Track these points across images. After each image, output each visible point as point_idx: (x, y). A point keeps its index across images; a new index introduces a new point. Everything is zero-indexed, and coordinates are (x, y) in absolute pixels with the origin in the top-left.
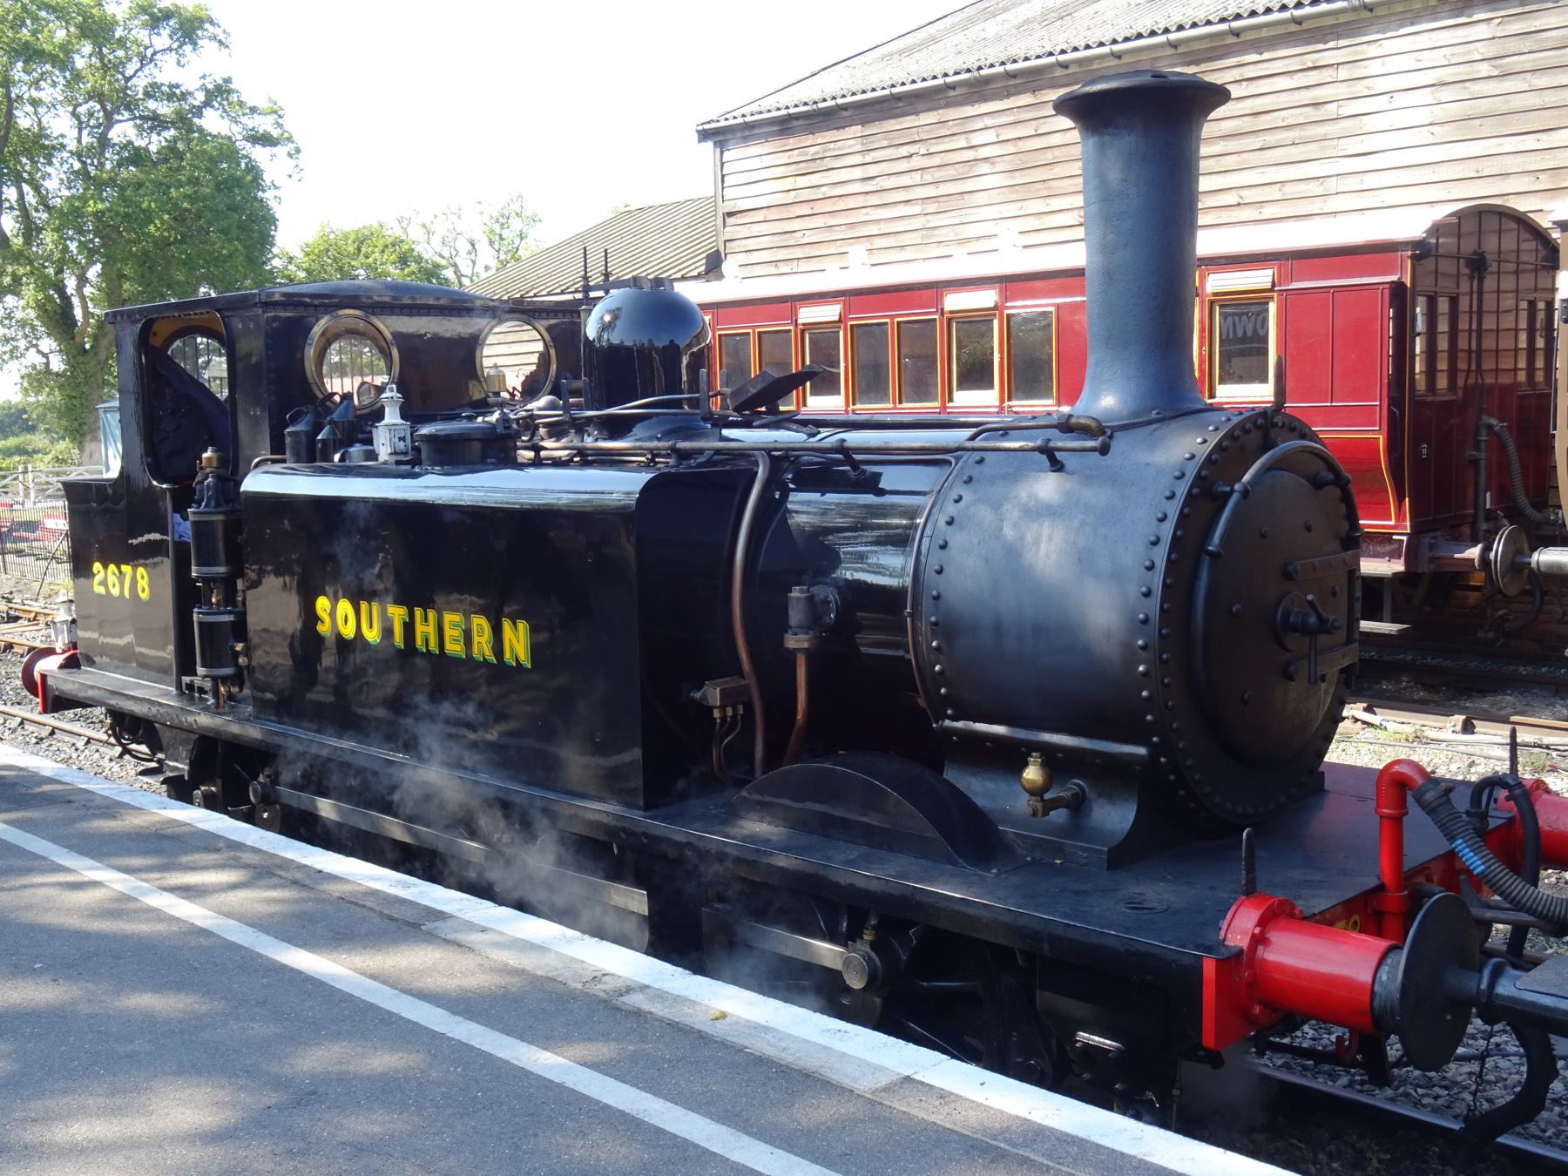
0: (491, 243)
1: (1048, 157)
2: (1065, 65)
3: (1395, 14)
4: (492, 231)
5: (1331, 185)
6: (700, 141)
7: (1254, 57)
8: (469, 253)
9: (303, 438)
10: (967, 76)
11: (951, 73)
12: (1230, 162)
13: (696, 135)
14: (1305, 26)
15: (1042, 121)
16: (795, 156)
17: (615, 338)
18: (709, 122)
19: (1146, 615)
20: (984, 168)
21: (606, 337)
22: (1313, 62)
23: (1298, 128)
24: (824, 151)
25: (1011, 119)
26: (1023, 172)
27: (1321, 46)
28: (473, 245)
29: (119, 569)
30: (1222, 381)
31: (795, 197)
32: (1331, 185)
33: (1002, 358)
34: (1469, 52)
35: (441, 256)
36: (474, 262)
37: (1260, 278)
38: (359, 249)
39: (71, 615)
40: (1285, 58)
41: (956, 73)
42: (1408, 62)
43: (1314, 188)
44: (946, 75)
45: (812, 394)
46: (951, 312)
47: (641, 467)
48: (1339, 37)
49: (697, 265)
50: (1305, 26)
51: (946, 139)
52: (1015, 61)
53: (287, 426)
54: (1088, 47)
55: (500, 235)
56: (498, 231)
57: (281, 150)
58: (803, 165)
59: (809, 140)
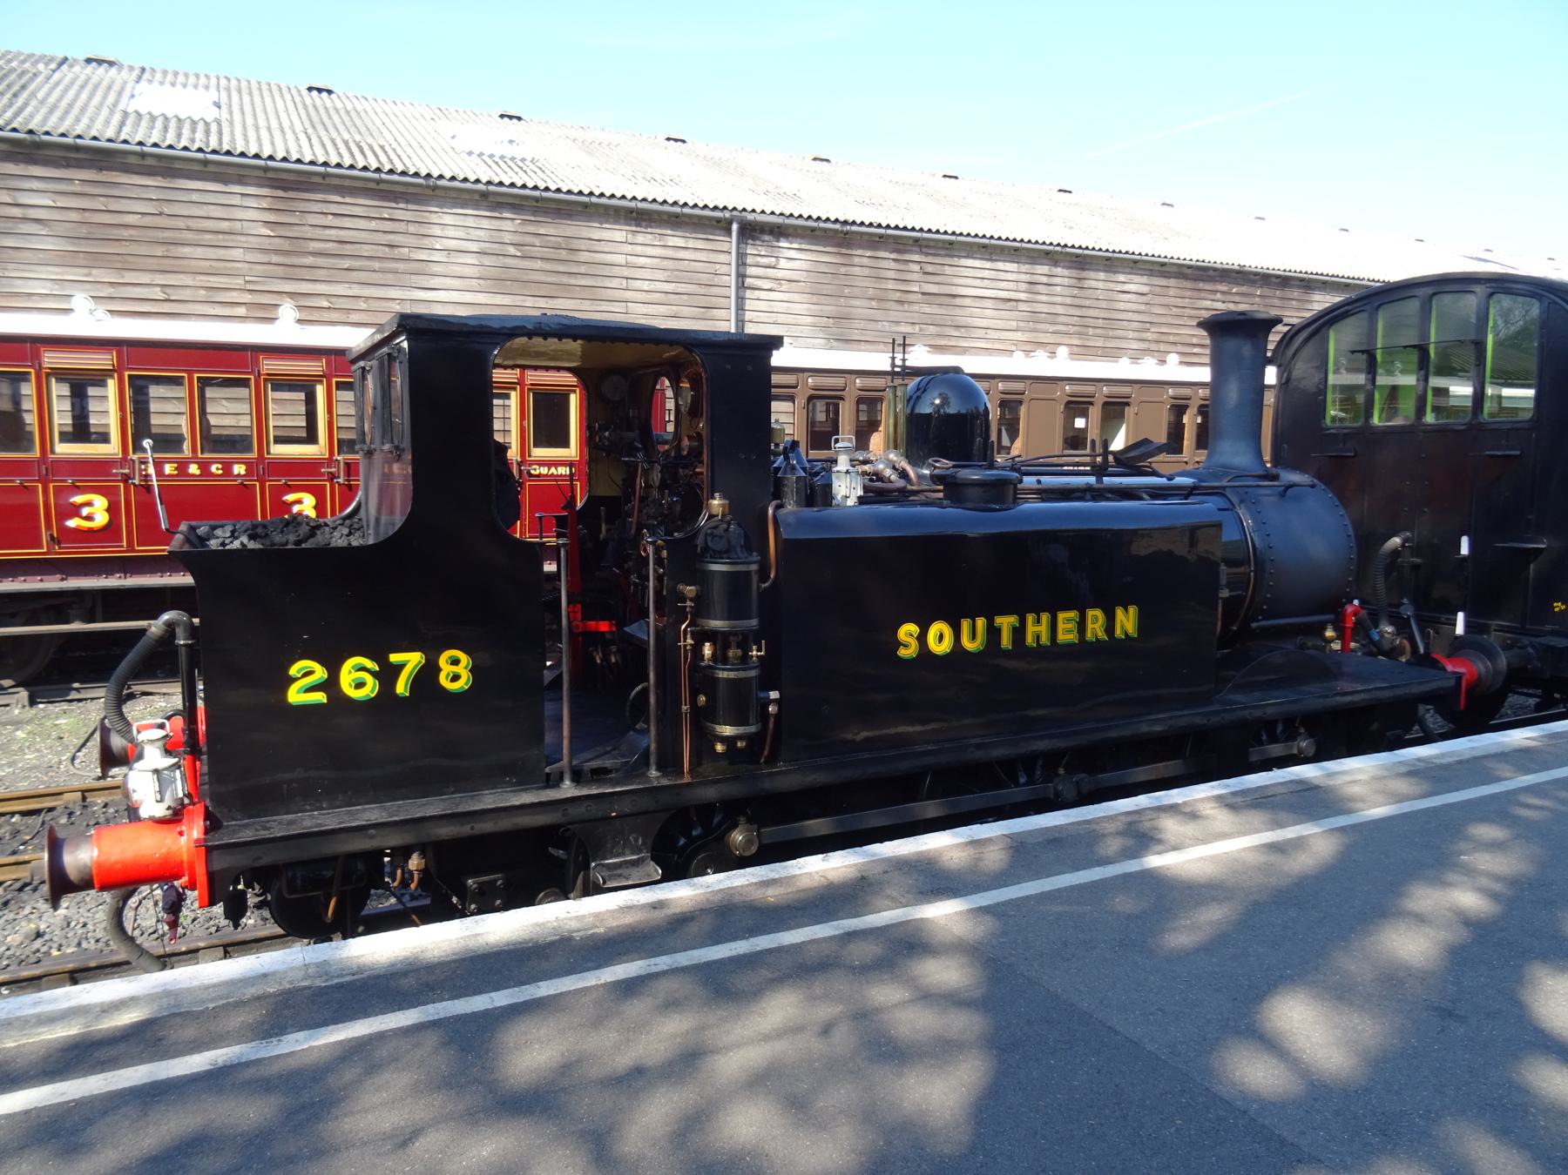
3: (450, 198)
7: (339, 199)
27: (394, 205)
40: (361, 205)
45: (534, 447)
48: (407, 202)
50: (328, 181)
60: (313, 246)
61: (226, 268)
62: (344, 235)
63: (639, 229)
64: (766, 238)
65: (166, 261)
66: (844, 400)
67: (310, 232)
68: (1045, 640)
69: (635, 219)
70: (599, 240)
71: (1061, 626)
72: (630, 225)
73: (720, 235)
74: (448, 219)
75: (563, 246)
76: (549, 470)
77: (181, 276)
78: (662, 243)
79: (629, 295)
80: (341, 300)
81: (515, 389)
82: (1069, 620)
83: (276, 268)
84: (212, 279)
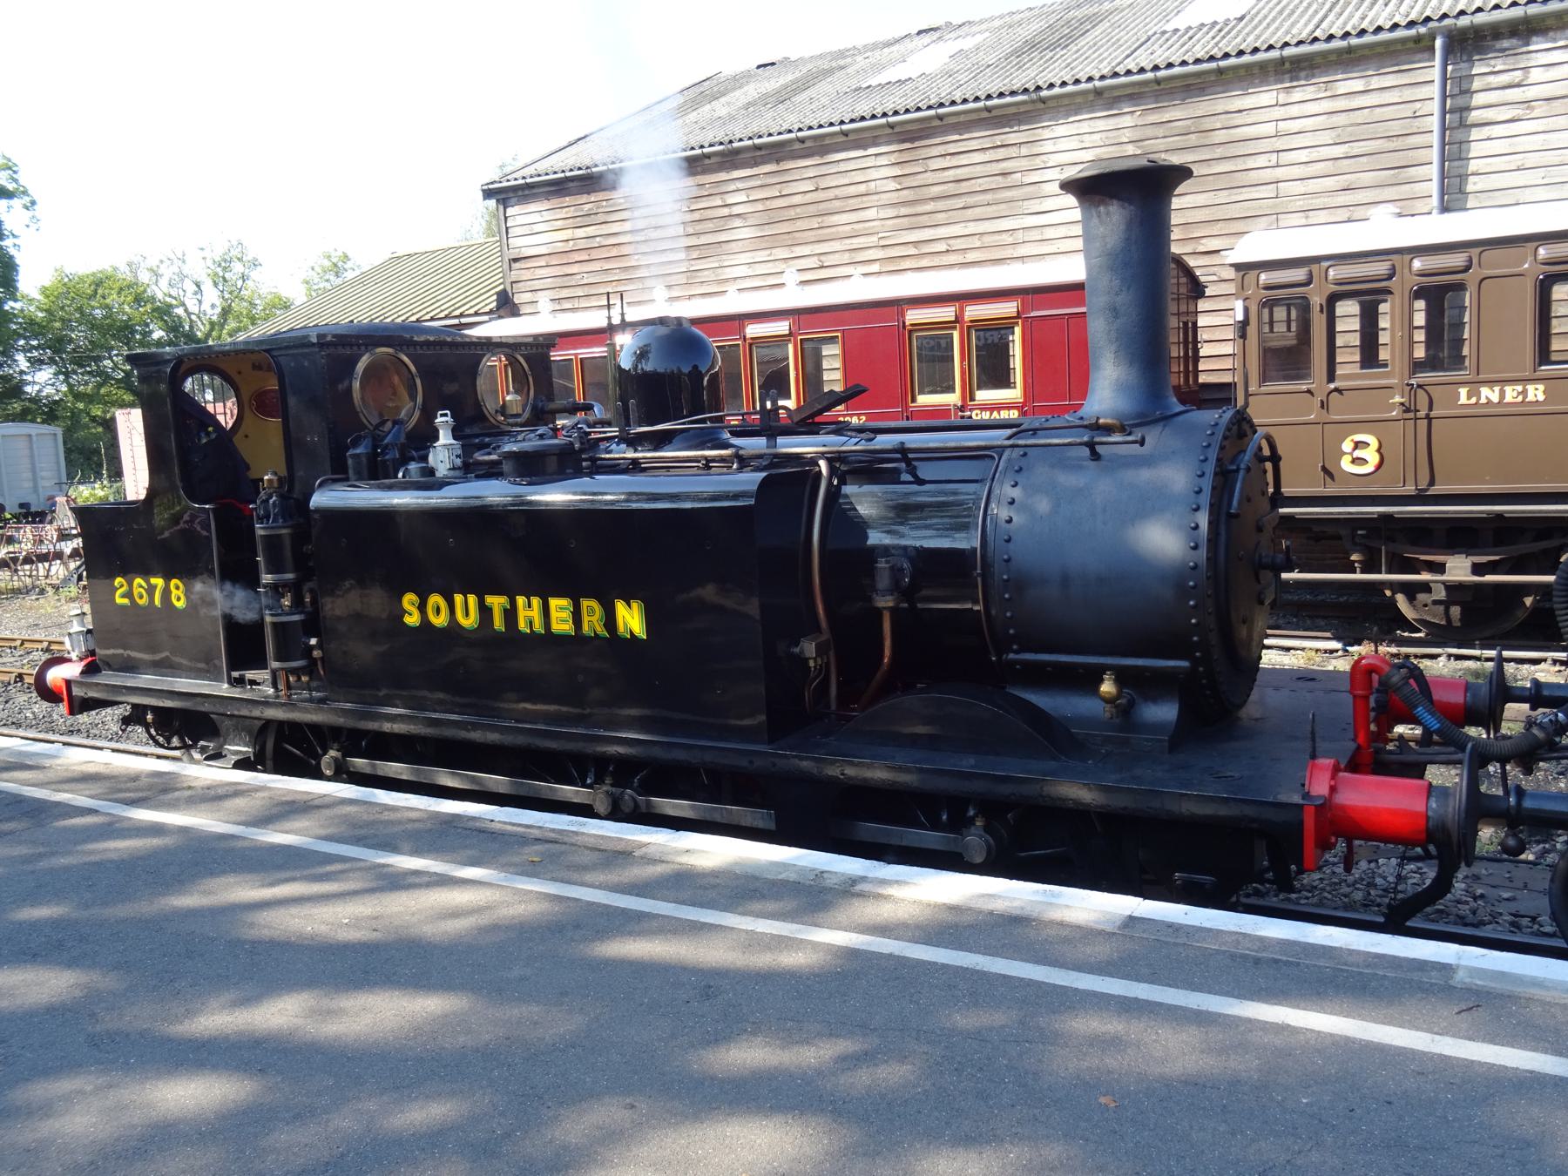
0: (216, 284)
1: (792, 213)
2: (802, 140)
4: (216, 274)
5: (1020, 236)
6: (485, 199)
8: (196, 293)
9: (364, 460)
10: (721, 147)
11: (706, 145)
12: (941, 217)
13: (481, 193)
14: (994, 113)
15: (784, 185)
16: (571, 212)
17: (648, 366)
18: (492, 183)
19: (1196, 563)
20: (738, 223)
21: (640, 367)
22: (1002, 141)
23: (991, 192)
24: (598, 208)
25: (759, 183)
26: (771, 226)
27: (1007, 130)
28: (198, 286)
29: (148, 582)
30: (979, 388)
31: (573, 246)
32: (1020, 236)
33: (797, 374)
34: (1119, 136)
35: (170, 296)
36: (200, 302)
37: (1008, 308)
38: (96, 292)
39: (84, 626)
40: (978, 139)
41: (711, 145)
42: (1074, 144)
43: (1007, 239)
44: (702, 147)
46: (752, 339)
47: (757, 469)
49: (487, 302)
51: (704, 199)
52: (760, 137)
53: (348, 449)
54: (821, 126)
55: (224, 278)
56: (221, 274)
57: (16, 203)
58: (578, 219)
59: (584, 198)
60: (936, 190)
61: (865, 229)
62: (961, 173)
63: (1295, 84)
64: (1506, 44)
65: (820, 232)
66: (1391, 293)
67: (930, 178)
68: (538, 627)
69: (1290, 71)
70: (1240, 111)
71: (554, 614)
72: (1282, 82)
73: (1419, 61)
74: (1061, 130)
75: (1193, 129)
76: (991, 414)
77: (832, 243)
78: (1328, 94)
79: (1280, 173)
80: (959, 241)
81: (955, 328)
82: (562, 608)
83: (906, 219)
84: (854, 241)
